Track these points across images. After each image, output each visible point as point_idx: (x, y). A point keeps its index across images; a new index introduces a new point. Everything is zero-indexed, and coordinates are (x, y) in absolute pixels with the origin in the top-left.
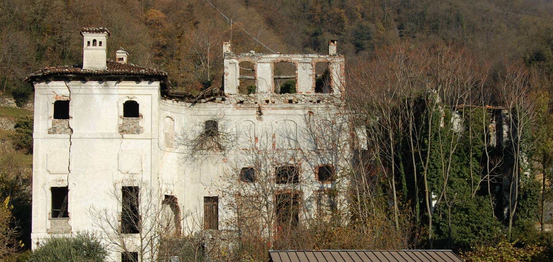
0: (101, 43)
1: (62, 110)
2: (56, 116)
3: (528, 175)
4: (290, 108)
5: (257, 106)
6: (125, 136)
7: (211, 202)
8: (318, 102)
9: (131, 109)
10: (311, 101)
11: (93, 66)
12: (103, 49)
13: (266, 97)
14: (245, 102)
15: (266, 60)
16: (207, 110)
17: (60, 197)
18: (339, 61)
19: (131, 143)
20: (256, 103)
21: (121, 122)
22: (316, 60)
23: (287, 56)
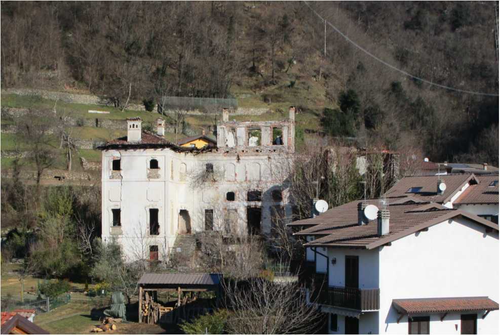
1: (117, 165)
2: (114, 169)
4: (257, 155)
5: (236, 154)
6: (151, 180)
7: (209, 213)
8: (275, 151)
9: (154, 164)
11: (134, 139)
12: (139, 130)
13: (242, 148)
14: (230, 152)
16: (208, 157)
17: (117, 213)
19: (155, 184)
20: (236, 152)
21: (149, 172)
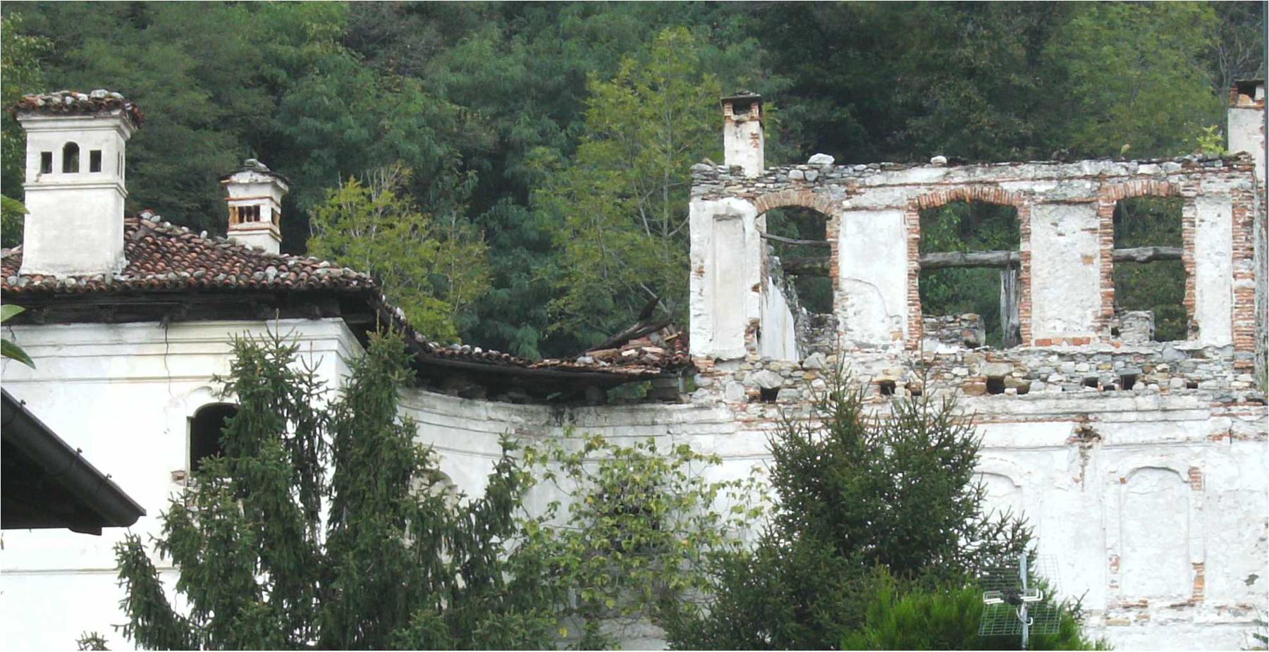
0: (96, 158)
3: (962, 542)
10: (1092, 383)
14: (784, 395)
15: (886, 197)
18: (1225, 187)
22: (1116, 191)
23: (979, 173)
